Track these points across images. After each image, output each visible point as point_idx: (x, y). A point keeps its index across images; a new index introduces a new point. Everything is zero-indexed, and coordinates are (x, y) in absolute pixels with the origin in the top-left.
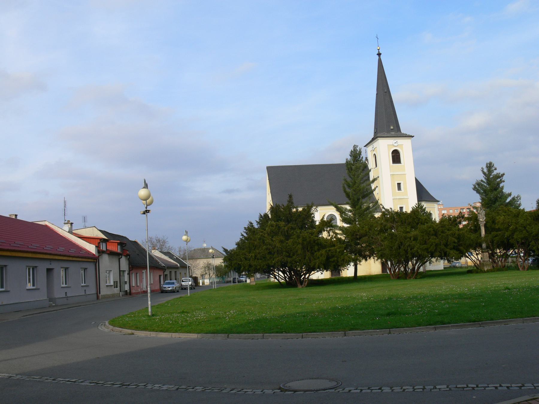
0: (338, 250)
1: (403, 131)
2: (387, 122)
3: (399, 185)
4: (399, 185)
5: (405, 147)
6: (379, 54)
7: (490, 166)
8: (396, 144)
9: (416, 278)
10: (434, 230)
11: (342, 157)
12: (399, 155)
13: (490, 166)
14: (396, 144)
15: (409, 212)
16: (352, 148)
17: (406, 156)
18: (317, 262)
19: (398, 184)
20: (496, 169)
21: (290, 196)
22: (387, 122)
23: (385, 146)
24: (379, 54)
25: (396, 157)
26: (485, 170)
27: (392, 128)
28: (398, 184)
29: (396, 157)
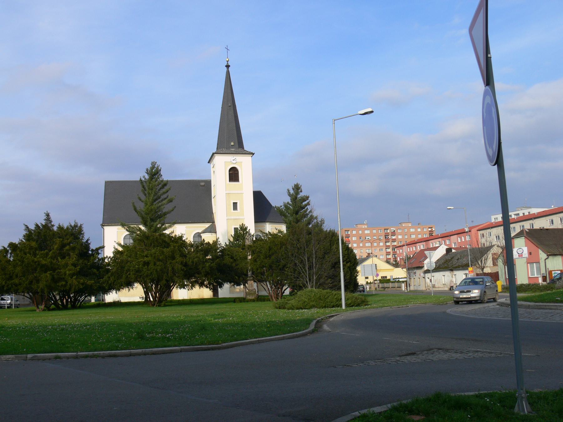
0: (68, 272)
1: (246, 147)
2: (231, 138)
3: (235, 204)
4: (235, 204)
5: (244, 164)
6: (228, 66)
7: (297, 188)
8: (234, 162)
9: (159, 306)
10: (20, 261)
11: (139, 174)
12: (238, 173)
13: (297, 188)
14: (234, 162)
15: (325, 230)
16: (149, 166)
17: (246, 175)
18: (133, 280)
19: (234, 203)
20: (301, 191)
21: (48, 215)
22: (231, 138)
23: (223, 163)
24: (228, 66)
25: (234, 175)
26: (292, 192)
27: (232, 144)
28: (234, 203)
29: (234, 175)
